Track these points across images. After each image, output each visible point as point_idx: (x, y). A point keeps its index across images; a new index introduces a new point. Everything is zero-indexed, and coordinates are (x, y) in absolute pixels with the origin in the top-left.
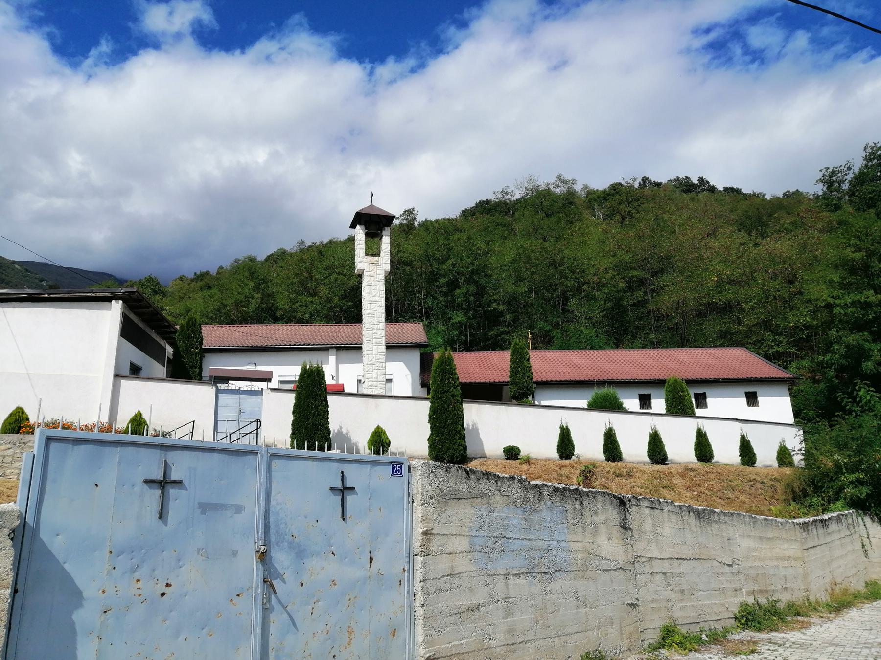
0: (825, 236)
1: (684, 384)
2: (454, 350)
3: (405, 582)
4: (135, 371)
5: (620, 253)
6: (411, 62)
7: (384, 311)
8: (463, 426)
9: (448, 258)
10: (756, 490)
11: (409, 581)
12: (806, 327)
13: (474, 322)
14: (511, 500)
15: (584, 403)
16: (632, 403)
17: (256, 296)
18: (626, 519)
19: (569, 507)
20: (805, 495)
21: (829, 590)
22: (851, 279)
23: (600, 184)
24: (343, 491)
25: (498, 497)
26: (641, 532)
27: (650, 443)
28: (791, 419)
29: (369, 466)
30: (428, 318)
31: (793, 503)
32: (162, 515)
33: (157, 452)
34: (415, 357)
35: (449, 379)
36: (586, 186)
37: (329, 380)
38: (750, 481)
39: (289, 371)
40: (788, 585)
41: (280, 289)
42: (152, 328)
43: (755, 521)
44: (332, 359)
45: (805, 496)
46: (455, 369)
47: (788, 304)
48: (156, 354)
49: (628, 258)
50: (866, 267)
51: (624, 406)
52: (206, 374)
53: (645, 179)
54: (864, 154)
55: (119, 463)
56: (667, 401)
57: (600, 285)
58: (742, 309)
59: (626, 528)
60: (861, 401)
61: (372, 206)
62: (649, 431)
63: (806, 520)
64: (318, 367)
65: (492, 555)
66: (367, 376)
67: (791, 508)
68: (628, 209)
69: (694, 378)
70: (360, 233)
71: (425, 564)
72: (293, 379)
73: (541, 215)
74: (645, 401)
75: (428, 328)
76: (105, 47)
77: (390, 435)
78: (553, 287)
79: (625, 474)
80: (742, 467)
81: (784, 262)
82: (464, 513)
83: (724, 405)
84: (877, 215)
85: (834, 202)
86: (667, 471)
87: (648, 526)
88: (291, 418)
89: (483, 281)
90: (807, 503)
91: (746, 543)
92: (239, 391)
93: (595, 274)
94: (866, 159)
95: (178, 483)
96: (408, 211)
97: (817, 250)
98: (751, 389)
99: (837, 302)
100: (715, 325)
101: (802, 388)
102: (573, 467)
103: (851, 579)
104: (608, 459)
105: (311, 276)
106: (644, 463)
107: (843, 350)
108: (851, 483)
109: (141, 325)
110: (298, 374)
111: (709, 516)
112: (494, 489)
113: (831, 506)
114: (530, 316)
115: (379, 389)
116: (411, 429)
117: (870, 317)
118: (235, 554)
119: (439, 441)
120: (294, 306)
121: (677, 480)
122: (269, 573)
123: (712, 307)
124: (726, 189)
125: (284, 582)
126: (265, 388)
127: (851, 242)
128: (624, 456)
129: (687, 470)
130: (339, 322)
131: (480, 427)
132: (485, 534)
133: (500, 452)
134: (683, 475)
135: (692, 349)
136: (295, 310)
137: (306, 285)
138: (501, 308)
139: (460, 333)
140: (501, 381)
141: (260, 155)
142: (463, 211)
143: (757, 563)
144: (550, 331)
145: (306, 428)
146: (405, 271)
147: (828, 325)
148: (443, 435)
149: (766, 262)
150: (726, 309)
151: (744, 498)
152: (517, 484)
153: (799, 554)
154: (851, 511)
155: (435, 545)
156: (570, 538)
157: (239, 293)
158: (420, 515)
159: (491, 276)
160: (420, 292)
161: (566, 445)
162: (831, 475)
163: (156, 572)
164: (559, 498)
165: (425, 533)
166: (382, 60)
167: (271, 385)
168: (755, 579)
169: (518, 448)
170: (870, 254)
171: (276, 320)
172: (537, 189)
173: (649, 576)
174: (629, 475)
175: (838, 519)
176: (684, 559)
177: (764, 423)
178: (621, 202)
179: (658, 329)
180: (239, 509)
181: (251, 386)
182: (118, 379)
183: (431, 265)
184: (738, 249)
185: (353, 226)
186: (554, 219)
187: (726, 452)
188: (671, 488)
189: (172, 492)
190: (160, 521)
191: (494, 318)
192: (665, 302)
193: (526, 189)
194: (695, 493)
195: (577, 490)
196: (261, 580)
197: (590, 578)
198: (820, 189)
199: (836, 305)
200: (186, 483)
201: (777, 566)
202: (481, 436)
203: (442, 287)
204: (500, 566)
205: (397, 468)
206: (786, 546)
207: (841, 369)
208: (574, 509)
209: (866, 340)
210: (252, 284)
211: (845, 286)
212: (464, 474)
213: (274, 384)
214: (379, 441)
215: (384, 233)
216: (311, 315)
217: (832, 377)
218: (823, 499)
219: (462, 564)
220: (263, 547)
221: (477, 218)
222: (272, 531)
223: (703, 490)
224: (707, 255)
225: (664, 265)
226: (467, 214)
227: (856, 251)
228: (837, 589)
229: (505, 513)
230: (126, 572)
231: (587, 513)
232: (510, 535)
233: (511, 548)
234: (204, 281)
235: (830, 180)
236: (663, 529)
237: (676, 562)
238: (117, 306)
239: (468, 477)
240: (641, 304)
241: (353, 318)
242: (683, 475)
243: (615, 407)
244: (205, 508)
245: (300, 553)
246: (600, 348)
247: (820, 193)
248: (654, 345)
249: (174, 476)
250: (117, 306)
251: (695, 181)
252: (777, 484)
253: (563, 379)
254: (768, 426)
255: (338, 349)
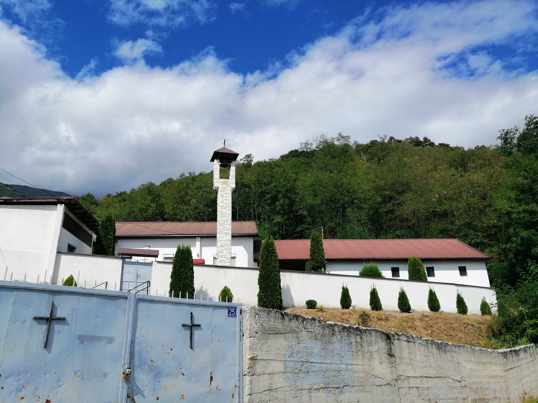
0: (504, 171)
1: (420, 261)
2: (275, 239)
3: (236, 396)
4: (71, 250)
5: (377, 180)
6: (269, 74)
7: (231, 213)
8: (280, 286)
9: (272, 182)
10: (469, 330)
11: (239, 394)
12: (494, 226)
13: (287, 222)
14: (313, 335)
15: (357, 273)
16: (387, 273)
17: (152, 205)
18: (391, 349)
19: (353, 340)
20: (501, 333)
21: (522, 398)
22: (522, 196)
23: (365, 141)
24: (192, 327)
25: (304, 332)
26: (401, 358)
27: (399, 299)
28: (488, 285)
29: (211, 309)
30: (259, 220)
31: (493, 339)
32: (47, 345)
33: (47, 296)
34: (250, 243)
35: (271, 256)
36: (356, 142)
37: (195, 257)
38: (464, 324)
39: (169, 251)
40: (497, 395)
41: (168, 201)
42: (84, 222)
43: (474, 351)
44: (198, 243)
45: (501, 335)
46: (275, 250)
47: (482, 212)
48: (86, 239)
49: (382, 183)
50: (531, 189)
51: (382, 275)
52: (116, 252)
53: (391, 138)
54: (525, 122)
55: (14, 304)
56: (409, 272)
57: (365, 200)
58: (454, 216)
59: (391, 355)
60: (532, 273)
61: (224, 148)
62: (398, 291)
63: (506, 350)
64: (188, 248)
65: (299, 375)
66: (219, 254)
67: (492, 342)
68: (382, 154)
69: (426, 257)
70: (217, 164)
71: (251, 382)
72: (172, 256)
73: (329, 157)
74: (395, 272)
75: (259, 225)
76: (92, 65)
77: (233, 292)
78: (336, 201)
79: (384, 318)
80: (459, 315)
81: (479, 186)
82: (279, 344)
83: (445, 275)
84: (536, 157)
85: (509, 150)
86: (411, 317)
87: (406, 354)
88: (170, 280)
89: (293, 196)
90: (502, 339)
91: (470, 366)
92: (137, 263)
93: (362, 193)
94: (526, 125)
95: (62, 320)
96: (248, 155)
97: (500, 179)
98: (462, 265)
99: (514, 210)
100: (436, 225)
101: (493, 264)
102: (350, 314)
103: (534, 390)
104: (373, 309)
105: (186, 193)
106: (396, 312)
107: (519, 241)
108: (531, 326)
109: (76, 220)
110: (175, 253)
111: (445, 347)
112: (301, 326)
113: (519, 341)
114: (322, 219)
115: (226, 263)
116: (247, 289)
117: (535, 220)
118: (105, 375)
119: (265, 296)
120: (176, 212)
121: (418, 323)
122: (132, 391)
123: (435, 214)
124: (441, 145)
125: (144, 396)
126: (154, 261)
127: (521, 174)
128: (383, 307)
129: (423, 317)
130: (204, 221)
131: (291, 288)
132: (295, 359)
133: (304, 304)
134: (421, 320)
135: (424, 240)
136: (176, 214)
137: (183, 200)
138: (305, 213)
139: (279, 229)
140: (305, 258)
141: (174, 127)
142: (281, 156)
143: (479, 380)
144: (334, 228)
145: (179, 287)
146: (245, 190)
147: (508, 225)
148: (267, 292)
149: (469, 187)
150: (444, 215)
151: (461, 335)
152: (317, 323)
153: (502, 373)
154: (532, 345)
155: (259, 367)
156: (354, 362)
157: (142, 204)
158: (248, 345)
159: (298, 193)
160: (254, 204)
161: (346, 299)
162: (517, 320)
163: (38, 391)
164: (346, 334)
165: (252, 359)
166: (252, 72)
167: (158, 259)
168: (476, 391)
169: (315, 302)
170: (534, 181)
171: (165, 220)
172: (326, 142)
173: (407, 389)
174: (387, 319)
175: (525, 350)
176: (430, 377)
177: (470, 287)
178: (378, 151)
179: (401, 227)
180: (110, 340)
181: (145, 260)
182: (60, 254)
183: (261, 187)
184: (451, 178)
185: (212, 160)
186: (336, 159)
187: (448, 305)
188: (414, 328)
189: (57, 327)
190: (45, 350)
191: (300, 220)
192: (406, 211)
193: (320, 141)
194: (430, 332)
195: (358, 328)
196: (125, 396)
197: (368, 391)
198: (499, 143)
199: (513, 213)
200: (68, 320)
201: (489, 382)
202: (292, 294)
203: (267, 200)
204: (305, 382)
205: (232, 311)
206: (494, 368)
207: (517, 254)
208: (356, 342)
209: (534, 235)
210: (150, 198)
211: (519, 201)
212: (280, 316)
213: (160, 258)
214: (226, 295)
215: (232, 164)
216: (186, 217)
217: (511, 259)
218: (513, 336)
219: (279, 382)
220: (128, 370)
221: (289, 160)
222: (136, 357)
223: (434, 329)
224: (431, 182)
225: (405, 189)
226: (284, 158)
227: (524, 179)
228: (527, 397)
229: (309, 344)
230: (11, 392)
231: (365, 344)
232: (313, 360)
233: (313, 369)
234: (122, 197)
235: (506, 137)
236: (416, 356)
237: (425, 379)
238: (61, 208)
239: (283, 318)
240: (392, 211)
241: (213, 219)
242: (421, 320)
243: (377, 275)
244: (83, 339)
245: (157, 374)
246: (366, 238)
247: (500, 145)
248: (398, 237)
249: (59, 315)
250: (61, 208)
251: (422, 139)
252: (482, 326)
253: (344, 258)
254: (474, 288)
255: (202, 237)
